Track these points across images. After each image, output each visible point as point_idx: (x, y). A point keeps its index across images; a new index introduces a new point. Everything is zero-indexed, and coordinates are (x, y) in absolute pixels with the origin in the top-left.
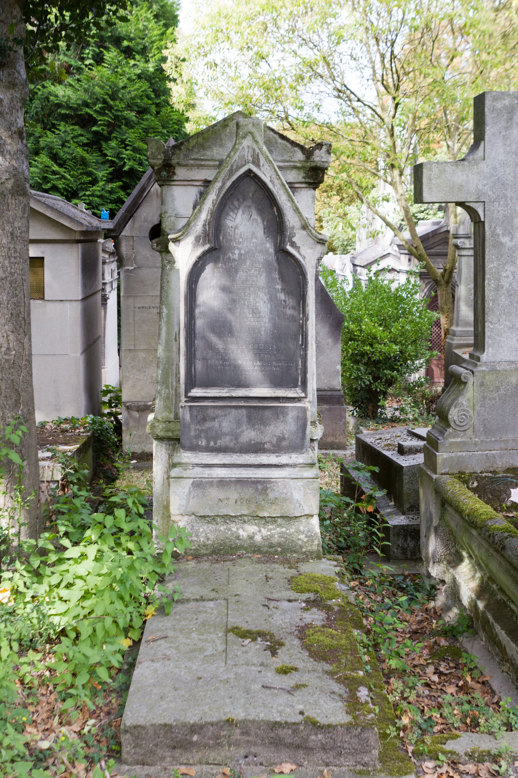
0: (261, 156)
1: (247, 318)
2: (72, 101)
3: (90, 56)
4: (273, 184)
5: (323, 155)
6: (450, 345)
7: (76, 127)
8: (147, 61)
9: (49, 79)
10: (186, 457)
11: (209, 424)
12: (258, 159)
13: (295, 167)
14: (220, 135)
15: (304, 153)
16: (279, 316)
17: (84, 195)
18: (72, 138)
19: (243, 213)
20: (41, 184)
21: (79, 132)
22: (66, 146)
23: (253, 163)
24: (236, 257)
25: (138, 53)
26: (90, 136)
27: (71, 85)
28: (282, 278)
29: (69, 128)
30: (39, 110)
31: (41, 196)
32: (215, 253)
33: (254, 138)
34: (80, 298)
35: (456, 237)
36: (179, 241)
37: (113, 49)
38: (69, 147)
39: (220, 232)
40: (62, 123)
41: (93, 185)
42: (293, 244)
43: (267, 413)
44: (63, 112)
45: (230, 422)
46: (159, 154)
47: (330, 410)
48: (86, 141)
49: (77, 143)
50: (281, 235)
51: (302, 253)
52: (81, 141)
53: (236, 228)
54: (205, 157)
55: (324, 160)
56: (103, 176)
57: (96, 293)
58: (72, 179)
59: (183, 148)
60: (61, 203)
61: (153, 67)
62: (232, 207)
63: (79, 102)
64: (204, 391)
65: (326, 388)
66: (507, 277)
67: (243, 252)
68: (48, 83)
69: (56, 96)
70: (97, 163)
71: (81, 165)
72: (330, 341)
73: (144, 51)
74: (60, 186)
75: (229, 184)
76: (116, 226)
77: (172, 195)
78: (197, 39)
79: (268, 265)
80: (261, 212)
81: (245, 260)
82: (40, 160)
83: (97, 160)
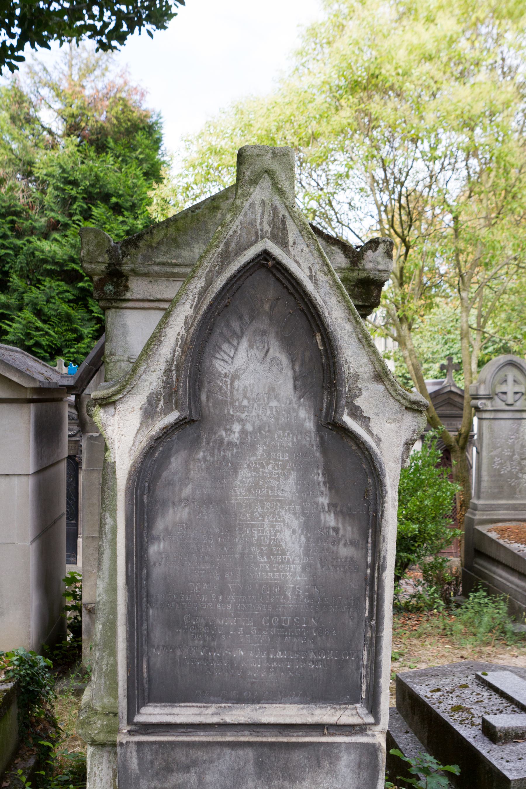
0: (290, 225)
1: (257, 564)
2: (58, 257)
3: (77, 211)
4: (316, 283)
5: (380, 259)
6: (471, 521)
7: (62, 283)
8: (136, 218)
9: (36, 235)
12: (285, 229)
14: (205, 223)
15: (347, 256)
16: (322, 560)
18: (58, 294)
19: (251, 346)
20: (24, 341)
21: (65, 288)
22: (51, 302)
23: (274, 237)
24: (235, 437)
25: (127, 210)
26: (76, 292)
27: (56, 240)
28: (332, 482)
29: (54, 284)
30: (24, 265)
32: (190, 430)
33: (275, 183)
34: (31, 472)
35: (476, 397)
36: (114, 403)
37: (102, 205)
38: (54, 303)
39: (200, 386)
40: (48, 279)
41: (79, 342)
42: (356, 413)
43: (297, 756)
44: (49, 267)
45: (221, 773)
46: (100, 255)
48: (71, 297)
49: (62, 299)
50: (331, 393)
51: (375, 431)
52: (66, 297)
53: (235, 376)
54: (180, 261)
55: (380, 267)
56: (89, 333)
57: (58, 462)
58: (56, 336)
59: (141, 244)
60: (18, 355)
61: (142, 224)
62: (228, 334)
63: (65, 257)
64: (167, 710)
67: (249, 428)
69: (42, 251)
70: (82, 320)
71: (66, 321)
73: (133, 207)
74: (44, 343)
75: (220, 282)
76: (77, 382)
77: (124, 326)
78: (186, 180)
79: (301, 455)
80: (288, 343)
81: (253, 447)
82: (22, 315)
83: (82, 316)
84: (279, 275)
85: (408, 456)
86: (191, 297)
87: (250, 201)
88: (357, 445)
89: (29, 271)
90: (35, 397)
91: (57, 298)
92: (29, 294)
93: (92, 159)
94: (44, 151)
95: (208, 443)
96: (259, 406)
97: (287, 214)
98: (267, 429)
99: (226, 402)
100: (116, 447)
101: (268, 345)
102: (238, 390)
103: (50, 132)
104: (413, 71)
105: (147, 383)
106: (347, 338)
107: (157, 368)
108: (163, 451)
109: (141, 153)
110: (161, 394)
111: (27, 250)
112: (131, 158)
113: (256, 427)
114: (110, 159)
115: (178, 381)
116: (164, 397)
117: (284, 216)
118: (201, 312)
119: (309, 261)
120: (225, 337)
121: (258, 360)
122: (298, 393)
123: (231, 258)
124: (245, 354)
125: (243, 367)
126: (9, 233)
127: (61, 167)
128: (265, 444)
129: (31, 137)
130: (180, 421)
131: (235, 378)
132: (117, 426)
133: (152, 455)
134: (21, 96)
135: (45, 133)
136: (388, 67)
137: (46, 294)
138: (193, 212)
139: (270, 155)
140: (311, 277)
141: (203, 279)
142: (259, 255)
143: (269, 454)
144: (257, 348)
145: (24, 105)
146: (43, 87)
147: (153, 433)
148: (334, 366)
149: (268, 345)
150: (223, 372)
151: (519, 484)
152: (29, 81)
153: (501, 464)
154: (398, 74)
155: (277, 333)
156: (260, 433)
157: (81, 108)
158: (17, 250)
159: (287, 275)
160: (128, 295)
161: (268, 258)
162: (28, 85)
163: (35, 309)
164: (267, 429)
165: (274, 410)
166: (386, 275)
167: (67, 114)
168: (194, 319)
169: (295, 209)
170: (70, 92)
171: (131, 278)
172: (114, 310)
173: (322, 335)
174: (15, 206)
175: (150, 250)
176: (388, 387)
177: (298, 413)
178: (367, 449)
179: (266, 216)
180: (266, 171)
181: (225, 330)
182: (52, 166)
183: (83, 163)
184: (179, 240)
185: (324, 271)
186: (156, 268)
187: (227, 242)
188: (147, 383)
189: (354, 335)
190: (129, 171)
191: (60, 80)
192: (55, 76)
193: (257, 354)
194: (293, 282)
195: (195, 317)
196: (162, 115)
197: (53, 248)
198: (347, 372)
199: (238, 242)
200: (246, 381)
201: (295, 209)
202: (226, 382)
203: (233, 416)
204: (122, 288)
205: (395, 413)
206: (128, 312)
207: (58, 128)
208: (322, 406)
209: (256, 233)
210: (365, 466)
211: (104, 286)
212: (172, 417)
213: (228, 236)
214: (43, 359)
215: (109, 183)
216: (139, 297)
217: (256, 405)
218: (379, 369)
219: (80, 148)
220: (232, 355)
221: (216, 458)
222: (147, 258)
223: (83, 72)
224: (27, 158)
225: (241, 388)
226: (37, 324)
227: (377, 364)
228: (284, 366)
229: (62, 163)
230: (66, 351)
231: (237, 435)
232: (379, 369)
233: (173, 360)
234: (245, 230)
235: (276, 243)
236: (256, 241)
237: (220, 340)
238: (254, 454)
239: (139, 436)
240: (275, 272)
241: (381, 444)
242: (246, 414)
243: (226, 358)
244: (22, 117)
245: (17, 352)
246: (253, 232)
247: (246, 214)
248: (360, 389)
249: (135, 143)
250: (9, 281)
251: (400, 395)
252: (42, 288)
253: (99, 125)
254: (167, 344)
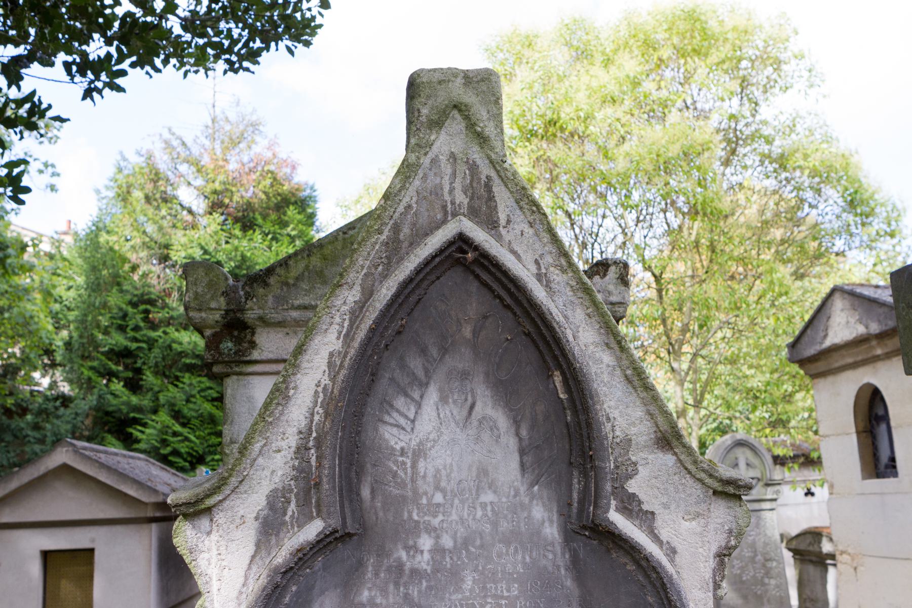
2: (199, 348)
4: (548, 286)
5: (611, 288)
7: (204, 379)
9: (173, 325)
12: (491, 198)
17: (213, 460)
18: (199, 392)
19: (444, 399)
20: (159, 449)
21: (208, 384)
22: (191, 402)
23: (473, 213)
24: (423, 561)
29: (195, 381)
30: (159, 360)
31: (93, 450)
32: (343, 551)
33: (471, 125)
36: (209, 510)
38: (195, 403)
39: (360, 474)
40: (187, 375)
42: (630, 505)
44: (188, 361)
46: (212, 298)
49: (204, 397)
50: (585, 474)
51: (664, 535)
52: (209, 395)
53: (419, 453)
55: (614, 299)
59: (272, 280)
62: (404, 380)
67: (447, 542)
68: (171, 330)
69: (181, 344)
71: (209, 424)
74: (183, 450)
75: (386, 291)
80: (506, 391)
81: (455, 576)
84: (485, 276)
85: (723, 577)
86: (337, 319)
87: (431, 155)
88: (637, 563)
89: (164, 367)
90: (158, 514)
91: (198, 396)
92: (165, 393)
93: (238, 238)
94: (183, 232)
95: (377, 575)
96: (462, 502)
97: (493, 174)
98: (478, 542)
99: (404, 498)
100: (214, 589)
101: (473, 397)
102: (424, 477)
103: (190, 211)
104: (596, 114)
105: (267, 473)
106: (606, 377)
107: (284, 444)
108: (297, 592)
109: (294, 229)
110: (291, 491)
111: (164, 342)
112: (282, 236)
113: (459, 541)
114: (258, 236)
115: (320, 466)
116: (297, 495)
117: (489, 178)
118: (356, 344)
119: (534, 250)
120: (399, 386)
121: (457, 424)
122: (529, 477)
123: (403, 251)
124: (434, 414)
125: (431, 437)
126: (142, 324)
127: (202, 248)
128: (475, 570)
129: (168, 217)
130: (327, 536)
131: (419, 456)
132: (215, 552)
133: (278, 600)
134: (157, 174)
135: (185, 212)
136: (568, 110)
137: (185, 392)
138: (345, 233)
139: (460, 80)
140: (539, 277)
141: (357, 288)
142: (450, 243)
143: (484, 588)
144: (455, 402)
145: (161, 183)
146: (181, 164)
147: (279, 560)
148: (589, 425)
149: (473, 397)
150: (398, 447)
151: (766, 591)
152: (166, 157)
153: (741, 568)
154: (579, 118)
155: (487, 374)
156: (467, 550)
157: (224, 183)
158: (151, 343)
159: (498, 274)
160: (256, 355)
161: (465, 247)
162: (165, 162)
163: (173, 410)
164: (478, 542)
165: (489, 508)
166: (621, 310)
167: (208, 190)
168: (345, 356)
169: (506, 165)
170: (212, 166)
171: (259, 330)
172: (235, 377)
173: (563, 374)
174: (149, 293)
175: (285, 289)
176: (682, 457)
177: (530, 512)
178: (654, 568)
179: (458, 180)
180: (455, 106)
181: (398, 374)
182: (192, 247)
183: (227, 242)
184: (326, 272)
185: (561, 266)
186: (295, 314)
187: (395, 224)
188: (267, 473)
189: (618, 372)
190: (280, 249)
191: (201, 155)
192: (196, 151)
193: (455, 412)
194: (510, 286)
195: (346, 353)
196: (316, 188)
197: (193, 338)
198: (610, 436)
199: (414, 224)
200: (439, 459)
201: (506, 165)
202: (404, 463)
203: (417, 522)
204: (246, 345)
205: (697, 503)
206: (255, 380)
207: (198, 207)
208: (571, 496)
209: (444, 207)
210: (650, 599)
211: (220, 342)
212: (313, 530)
213: (397, 215)
214: (182, 469)
215: (256, 264)
216: (271, 356)
217: (456, 501)
218: (664, 427)
219: (224, 227)
220: (412, 416)
221: (391, 600)
223: (226, 144)
224: (162, 240)
225: (431, 472)
226: (175, 428)
227: (660, 419)
228: (502, 431)
229: (203, 244)
230: (209, 458)
231: (426, 556)
232: (664, 427)
233: (310, 429)
234: (425, 204)
235: (477, 223)
236: (444, 222)
237: (390, 391)
238: (458, 589)
239: (254, 568)
240: (478, 271)
241: (678, 558)
242: (440, 517)
243: (402, 421)
244: (158, 196)
245: (139, 459)
246: (438, 207)
247: (425, 177)
248: (635, 464)
249: (286, 218)
250: (142, 379)
251: (704, 471)
252: (181, 385)
253: (245, 201)
254: (299, 402)
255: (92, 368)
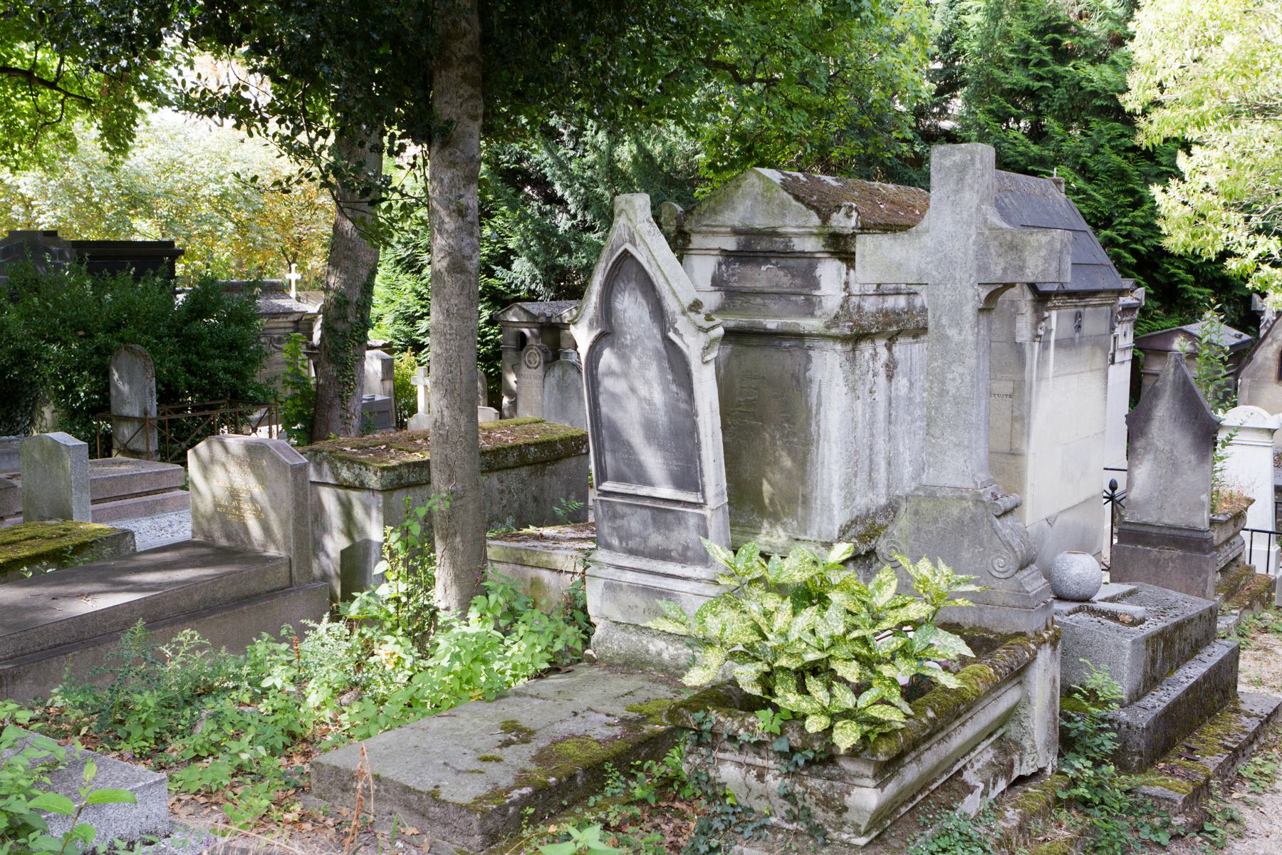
10: (602, 555)
11: (619, 522)
13: (812, 234)
18: (1109, 141)
42: (676, 331)
43: (670, 517)
44: (1099, 103)
47: (1184, 558)
53: (625, 311)
65: (1183, 525)
66: (954, 379)
72: (1193, 457)
79: (657, 351)
126: (1048, 58)
158: (1056, 79)
174: (1059, 18)
200: (629, 314)
222: (698, 222)
255: (990, 111)
